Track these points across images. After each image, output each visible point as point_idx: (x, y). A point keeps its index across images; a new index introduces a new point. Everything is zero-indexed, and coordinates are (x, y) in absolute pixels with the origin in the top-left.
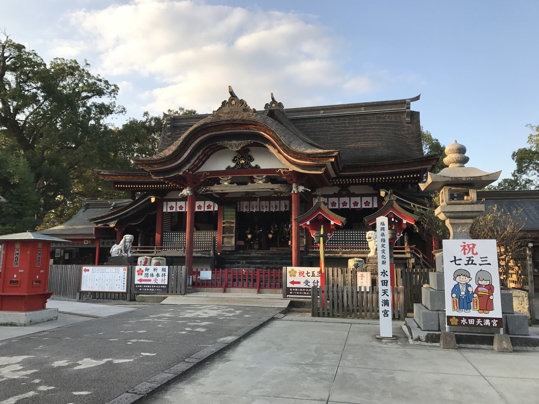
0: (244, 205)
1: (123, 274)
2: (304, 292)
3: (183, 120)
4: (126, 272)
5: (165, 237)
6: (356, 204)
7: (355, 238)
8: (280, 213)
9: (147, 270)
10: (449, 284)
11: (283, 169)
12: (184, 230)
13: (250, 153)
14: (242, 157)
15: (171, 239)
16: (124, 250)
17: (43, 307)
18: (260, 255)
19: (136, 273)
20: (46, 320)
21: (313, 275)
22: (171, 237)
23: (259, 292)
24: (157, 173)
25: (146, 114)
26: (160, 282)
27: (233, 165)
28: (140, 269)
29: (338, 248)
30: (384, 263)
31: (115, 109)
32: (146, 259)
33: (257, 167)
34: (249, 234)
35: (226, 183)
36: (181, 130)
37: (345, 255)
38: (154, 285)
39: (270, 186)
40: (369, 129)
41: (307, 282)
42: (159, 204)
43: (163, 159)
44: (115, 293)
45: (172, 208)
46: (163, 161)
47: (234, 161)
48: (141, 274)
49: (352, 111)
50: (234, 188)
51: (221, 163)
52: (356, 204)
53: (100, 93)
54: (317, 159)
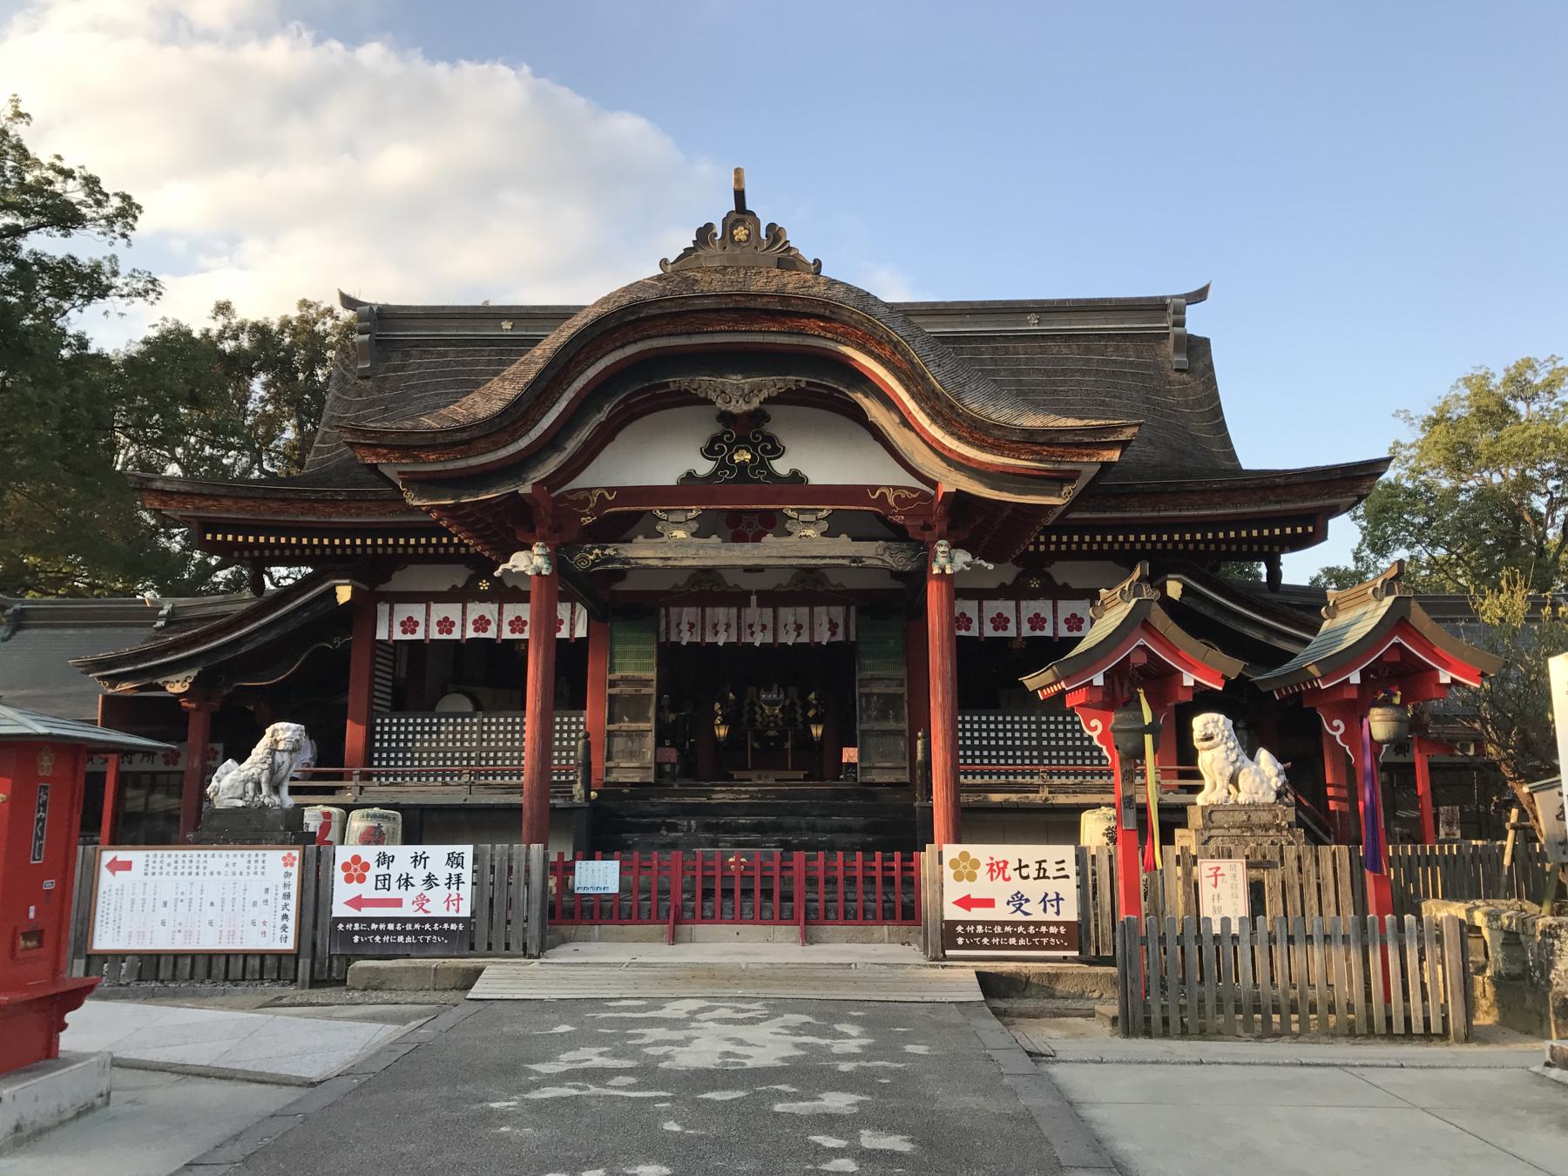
0: (685, 620)
1: (283, 880)
2: (1008, 936)
4: (295, 870)
5: (382, 733)
6: (1037, 622)
7: (1057, 739)
8: (812, 649)
11: (895, 488)
12: (107, 723)
13: (769, 428)
14: (743, 442)
15: (406, 741)
16: (270, 780)
17: (46, 1053)
18: (744, 799)
19: (339, 875)
20: (70, 1114)
21: (1042, 875)
22: (406, 733)
23: (807, 939)
24: (426, 483)
25: (223, 308)
26: (437, 909)
27: (704, 467)
28: (356, 859)
29: (1032, 774)
31: (118, 281)
32: (327, 815)
33: (796, 477)
34: (817, 720)
35: (680, 534)
36: (407, 355)
37: (1062, 799)
38: (413, 920)
39: (843, 547)
40: (1064, 383)
41: (1019, 900)
42: (363, 611)
43: (463, 429)
44: (246, 955)
45: (409, 626)
46: (465, 435)
47: (708, 452)
48: (362, 879)
49: (998, 323)
50: (712, 552)
51: (664, 459)
53: (65, 217)
54: (1058, 450)
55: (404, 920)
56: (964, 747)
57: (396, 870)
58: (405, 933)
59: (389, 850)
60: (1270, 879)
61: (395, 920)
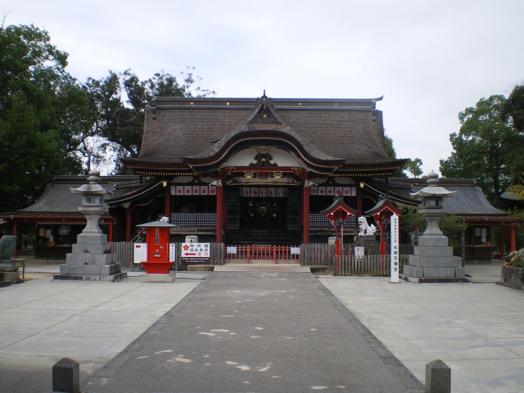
3: (166, 103)
8: (277, 199)
9: (192, 246)
23: (276, 263)
27: (255, 162)
28: (186, 246)
30: (395, 241)
33: (275, 164)
34: (251, 213)
38: (198, 258)
47: (256, 158)
48: (187, 249)
51: (244, 160)
55: (196, 258)
56: (311, 222)
57: (194, 248)
58: (196, 260)
59: (193, 244)
61: (194, 258)
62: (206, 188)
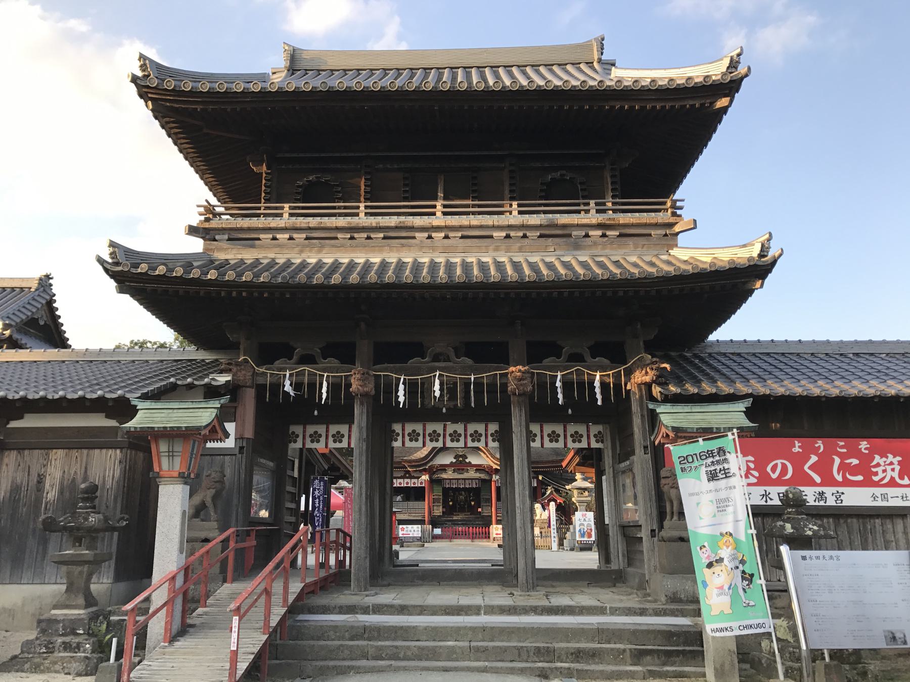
8: (472, 488)
10: (577, 529)
24: (411, 467)
27: (454, 461)
33: (470, 463)
45: (766, 495)
52: (400, 483)
60: (543, 531)
62: (416, 480)
